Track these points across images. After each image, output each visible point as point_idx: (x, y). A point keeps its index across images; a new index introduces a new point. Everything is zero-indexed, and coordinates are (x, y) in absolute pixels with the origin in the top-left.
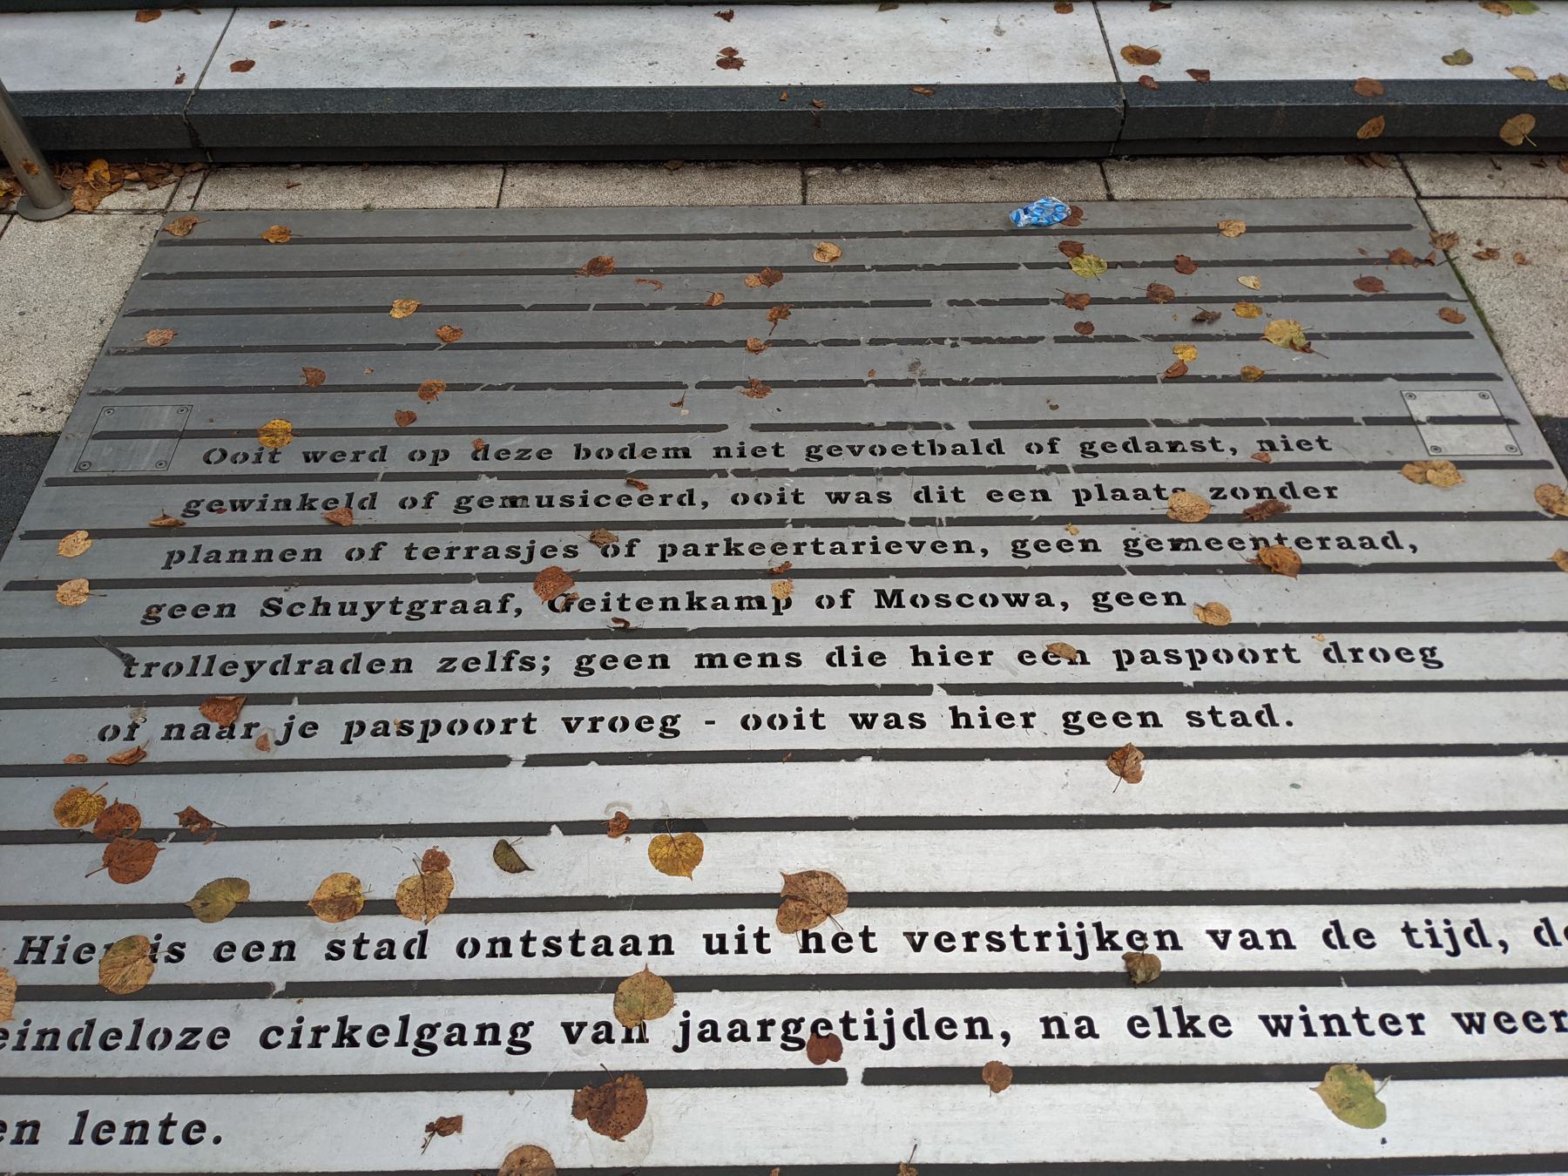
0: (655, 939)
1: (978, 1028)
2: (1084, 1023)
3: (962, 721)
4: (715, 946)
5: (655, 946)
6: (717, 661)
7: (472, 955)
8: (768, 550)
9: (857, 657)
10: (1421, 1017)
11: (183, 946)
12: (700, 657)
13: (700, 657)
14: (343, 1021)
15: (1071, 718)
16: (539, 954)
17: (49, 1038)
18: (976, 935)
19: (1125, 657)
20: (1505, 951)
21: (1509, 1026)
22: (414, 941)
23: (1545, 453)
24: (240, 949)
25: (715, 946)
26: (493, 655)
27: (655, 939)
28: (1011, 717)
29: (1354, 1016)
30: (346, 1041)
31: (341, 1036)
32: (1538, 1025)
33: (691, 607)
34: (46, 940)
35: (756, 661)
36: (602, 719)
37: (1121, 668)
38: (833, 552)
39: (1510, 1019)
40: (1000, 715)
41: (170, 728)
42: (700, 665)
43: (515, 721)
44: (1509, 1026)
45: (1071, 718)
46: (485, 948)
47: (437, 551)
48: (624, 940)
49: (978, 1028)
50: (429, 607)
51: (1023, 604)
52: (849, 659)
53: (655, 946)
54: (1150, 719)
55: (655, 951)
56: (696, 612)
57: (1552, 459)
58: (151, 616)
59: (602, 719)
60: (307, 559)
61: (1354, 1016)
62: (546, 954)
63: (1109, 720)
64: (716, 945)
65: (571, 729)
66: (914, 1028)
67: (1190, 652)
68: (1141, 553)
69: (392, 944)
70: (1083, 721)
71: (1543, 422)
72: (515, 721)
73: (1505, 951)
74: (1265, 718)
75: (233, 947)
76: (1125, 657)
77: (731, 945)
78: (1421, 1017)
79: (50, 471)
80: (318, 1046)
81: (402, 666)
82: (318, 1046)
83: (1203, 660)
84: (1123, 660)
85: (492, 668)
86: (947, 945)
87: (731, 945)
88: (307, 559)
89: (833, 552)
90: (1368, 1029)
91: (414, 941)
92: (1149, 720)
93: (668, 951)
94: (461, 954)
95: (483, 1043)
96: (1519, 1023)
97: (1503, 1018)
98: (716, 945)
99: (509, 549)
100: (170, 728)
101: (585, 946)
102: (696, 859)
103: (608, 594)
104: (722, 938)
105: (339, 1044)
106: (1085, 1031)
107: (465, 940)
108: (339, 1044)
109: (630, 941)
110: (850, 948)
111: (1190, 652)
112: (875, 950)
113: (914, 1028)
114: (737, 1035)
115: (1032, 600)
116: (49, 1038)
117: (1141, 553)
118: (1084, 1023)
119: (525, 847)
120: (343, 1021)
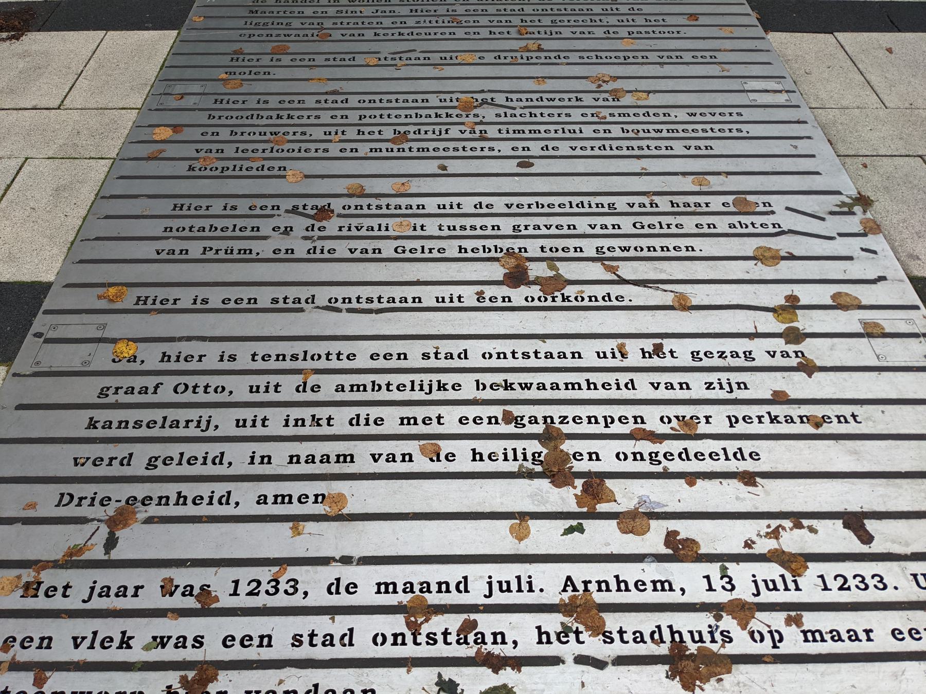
0: (440, 584)
1: (499, 638)
2: (638, 635)
3: (478, 457)
4: (505, 587)
5: (440, 588)
6: (412, 421)
7: (382, 644)
8: (381, 357)
9: (367, 420)
10: (871, 631)
11: (202, 637)
12: (402, 419)
13: (402, 419)
14: (124, 633)
15: (653, 455)
16: (424, 644)
17: (46, 641)
18: (590, 582)
19: (733, 420)
20: (683, 594)
21: (900, 636)
22: (333, 584)
23: (915, 300)
24: (19, 641)
25: (505, 587)
26: (413, 382)
27: (440, 584)
28: (581, 455)
29: (618, 632)
30: (124, 646)
31: (122, 642)
32: (917, 636)
33: (439, 389)
34: (147, 298)
35: (486, 421)
36: (116, 458)
37: (731, 426)
38: (546, 357)
39: (901, 633)
40: (491, 454)
41: (291, 457)
42: (402, 424)
43: (192, 421)
44: (900, 636)
45: (653, 455)
46: (390, 639)
47: (270, 356)
48: (405, 584)
49: (499, 638)
50: (112, 390)
51: (529, 389)
52: (362, 421)
53: (440, 588)
54: (638, 456)
55: (440, 591)
56: (442, 392)
57: (919, 302)
58: (103, 393)
59: (116, 458)
60: (277, 360)
61: (618, 632)
62: (428, 643)
63: (707, 456)
64: (505, 587)
65: (376, 461)
66: (462, 587)
67: (605, 417)
68: (701, 359)
69: (332, 636)
70: (660, 457)
71: (915, 281)
72: (192, 421)
73: (683, 594)
74: (739, 456)
75: (233, 639)
76: (733, 420)
77: (514, 587)
78: (871, 631)
79: (46, 305)
80: (137, 596)
81: (300, 423)
82: (137, 596)
83: (612, 422)
84: (733, 421)
85: (413, 389)
86: (642, 588)
87: (514, 587)
88: (277, 360)
89: (546, 357)
90: (625, 639)
91: (333, 584)
92: (294, 459)
93: (269, 645)
94: (375, 643)
95: (397, 644)
96: (906, 635)
97: (913, 632)
98: (505, 587)
99: (292, 356)
100: (291, 457)
101: (318, 640)
102: (526, 536)
103: (288, 416)
104: (508, 583)
105: (120, 647)
106: (639, 640)
107: (377, 635)
108: (120, 647)
109: (328, 637)
110: (568, 642)
111: (605, 417)
112: (583, 643)
113: (462, 587)
114: (462, 641)
115: (534, 386)
116: (46, 641)
117: (701, 359)
118: (638, 635)
119: (871, 525)
120: (124, 633)
